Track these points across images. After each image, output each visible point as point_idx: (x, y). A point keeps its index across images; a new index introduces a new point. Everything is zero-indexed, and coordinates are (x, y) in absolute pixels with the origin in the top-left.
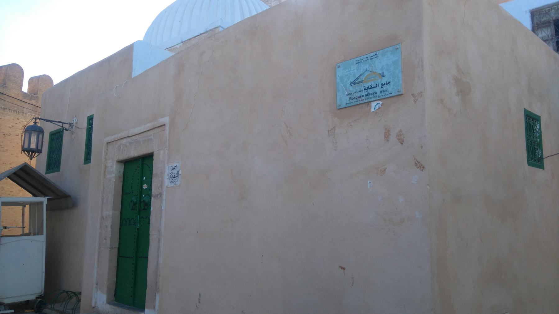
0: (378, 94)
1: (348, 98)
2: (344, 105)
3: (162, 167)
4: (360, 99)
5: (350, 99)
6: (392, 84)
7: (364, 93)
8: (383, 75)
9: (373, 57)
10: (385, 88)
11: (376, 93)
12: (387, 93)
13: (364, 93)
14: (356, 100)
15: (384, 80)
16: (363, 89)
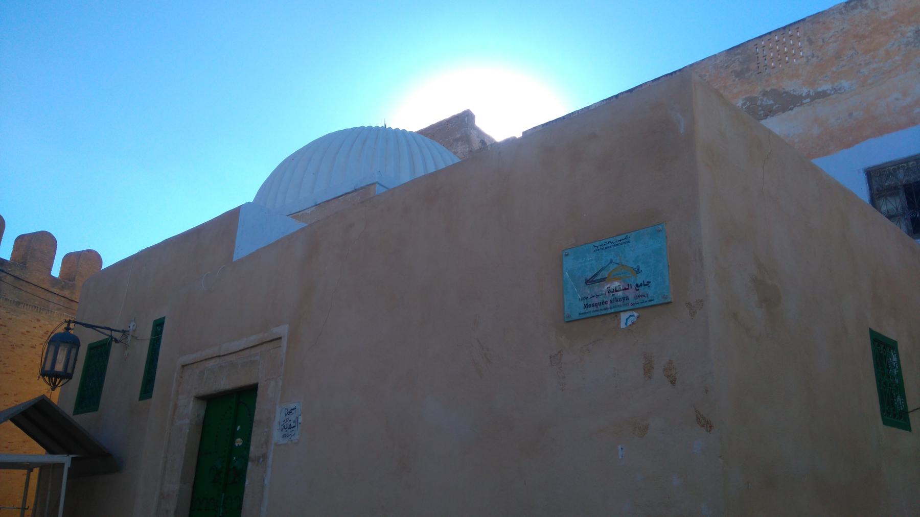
1: (582, 304)
2: (575, 316)
3: (271, 410)
4: (602, 307)
5: (586, 306)
6: (653, 284)
8: (638, 271)
10: (642, 290)
11: (628, 298)
12: (645, 299)
14: (595, 308)
15: (640, 279)
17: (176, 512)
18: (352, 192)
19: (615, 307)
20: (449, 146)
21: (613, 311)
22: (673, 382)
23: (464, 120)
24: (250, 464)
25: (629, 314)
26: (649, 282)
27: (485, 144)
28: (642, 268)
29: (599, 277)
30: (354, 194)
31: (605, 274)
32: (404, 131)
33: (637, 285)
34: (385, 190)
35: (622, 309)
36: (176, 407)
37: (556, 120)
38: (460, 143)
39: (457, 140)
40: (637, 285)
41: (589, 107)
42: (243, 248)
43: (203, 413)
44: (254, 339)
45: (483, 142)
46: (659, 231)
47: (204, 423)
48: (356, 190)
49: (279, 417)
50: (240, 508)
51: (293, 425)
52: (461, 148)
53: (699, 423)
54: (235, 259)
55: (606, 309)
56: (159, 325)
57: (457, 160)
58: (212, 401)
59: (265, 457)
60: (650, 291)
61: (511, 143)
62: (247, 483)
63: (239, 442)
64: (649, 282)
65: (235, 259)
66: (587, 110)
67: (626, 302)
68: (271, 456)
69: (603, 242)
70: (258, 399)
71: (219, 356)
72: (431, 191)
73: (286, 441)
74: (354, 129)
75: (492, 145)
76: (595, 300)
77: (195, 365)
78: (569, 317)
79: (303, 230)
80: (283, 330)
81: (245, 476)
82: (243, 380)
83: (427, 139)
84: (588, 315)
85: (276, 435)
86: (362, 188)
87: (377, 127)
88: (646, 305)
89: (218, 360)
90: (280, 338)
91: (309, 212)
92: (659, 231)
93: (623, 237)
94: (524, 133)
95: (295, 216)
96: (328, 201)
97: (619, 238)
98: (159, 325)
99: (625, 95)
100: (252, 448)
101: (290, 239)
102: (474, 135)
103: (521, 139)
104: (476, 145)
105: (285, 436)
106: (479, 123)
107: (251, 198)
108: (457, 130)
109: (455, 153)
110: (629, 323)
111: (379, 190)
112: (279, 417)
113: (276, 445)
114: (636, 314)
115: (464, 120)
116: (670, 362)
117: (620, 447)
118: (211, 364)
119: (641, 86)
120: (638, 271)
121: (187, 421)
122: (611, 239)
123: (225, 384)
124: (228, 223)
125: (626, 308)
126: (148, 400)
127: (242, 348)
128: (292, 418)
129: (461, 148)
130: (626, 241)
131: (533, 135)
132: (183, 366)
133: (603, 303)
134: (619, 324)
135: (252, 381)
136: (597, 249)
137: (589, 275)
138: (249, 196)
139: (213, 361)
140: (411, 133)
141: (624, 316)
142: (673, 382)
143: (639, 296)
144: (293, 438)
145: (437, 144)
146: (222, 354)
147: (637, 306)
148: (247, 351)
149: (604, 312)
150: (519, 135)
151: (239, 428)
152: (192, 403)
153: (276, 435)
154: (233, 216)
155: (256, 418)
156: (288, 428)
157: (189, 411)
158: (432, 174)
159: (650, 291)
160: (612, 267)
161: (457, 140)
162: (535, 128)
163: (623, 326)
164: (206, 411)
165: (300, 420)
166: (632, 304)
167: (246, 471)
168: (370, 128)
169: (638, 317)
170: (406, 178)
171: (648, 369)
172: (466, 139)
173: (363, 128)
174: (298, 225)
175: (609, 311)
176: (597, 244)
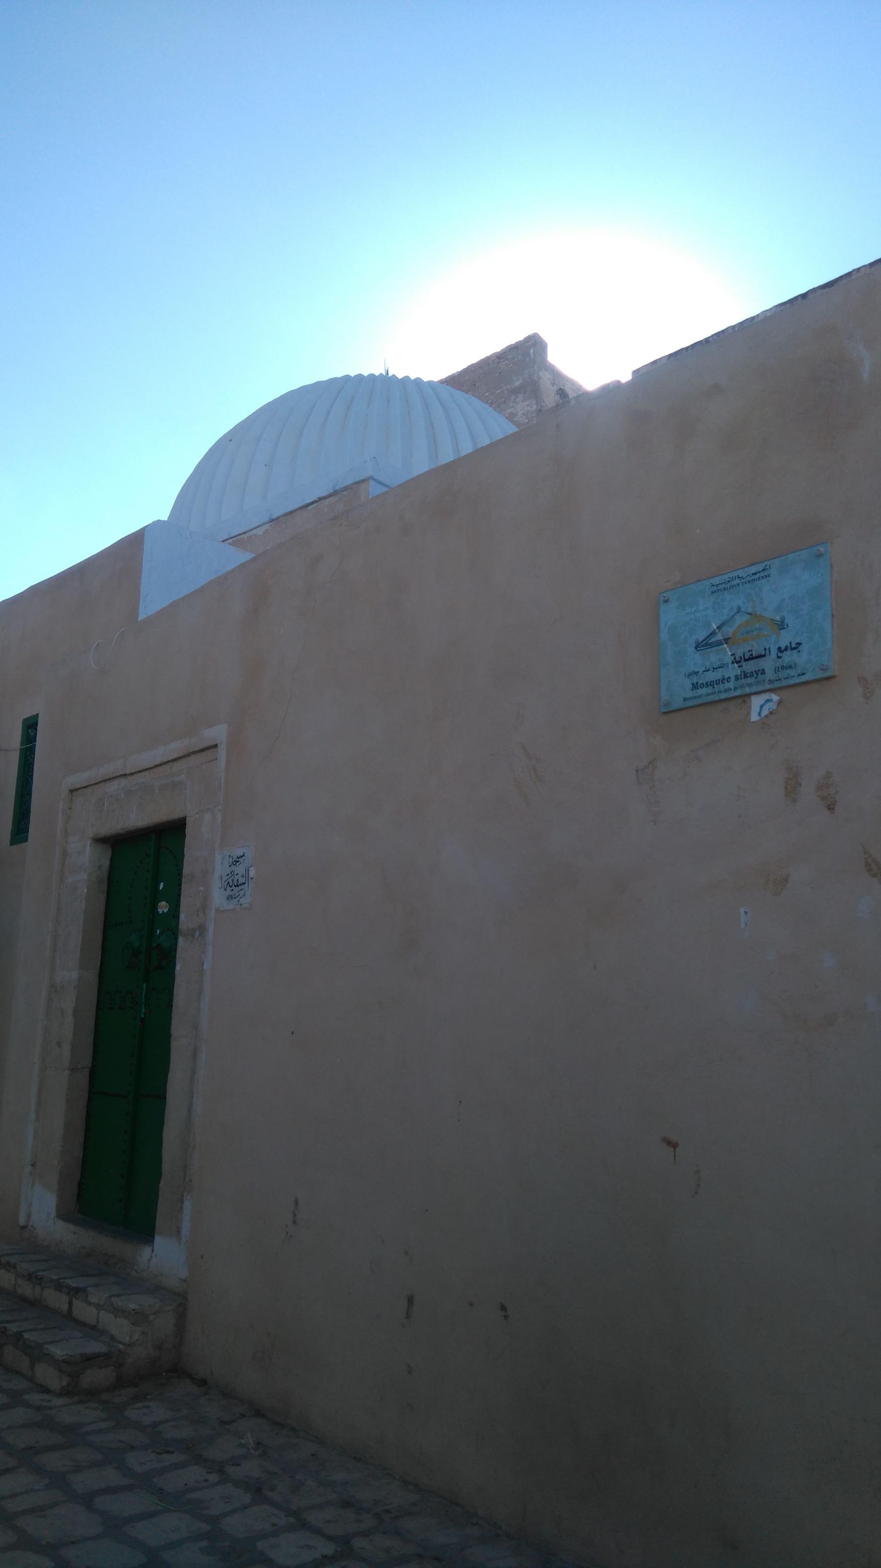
0: (770, 674)
1: (688, 684)
2: (678, 703)
3: (207, 857)
4: (722, 687)
5: (695, 686)
6: (805, 648)
7: (733, 671)
8: (782, 625)
9: (755, 578)
10: (787, 657)
11: (763, 672)
12: (791, 672)
13: (733, 671)
14: (709, 690)
15: (786, 638)
16: (729, 659)
17: (75, 1012)
18: (330, 496)
19: (742, 686)
20: (497, 403)
21: (738, 693)
22: (831, 808)
23: (527, 354)
24: (181, 940)
25: (765, 696)
26: (799, 644)
27: (565, 393)
28: (790, 620)
29: (719, 637)
30: (333, 500)
31: (729, 631)
32: (418, 382)
33: (779, 649)
34: (382, 490)
35: (754, 689)
36: (65, 854)
37: (693, 346)
38: (521, 396)
39: (516, 391)
40: (779, 649)
41: (753, 318)
42: (153, 599)
43: (106, 863)
44: (176, 747)
45: (562, 393)
46: (820, 555)
47: (109, 878)
48: (335, 493)
49: (220, 869)
50: (170, 1005)
51: (241, 880)
52: (523, 407)
53: (869, 870)
54: (142, 616)
55: (727, 690)
56: (31, 726)
57: (511, 429)
58: (119, 844)
59: (202, 929)
60: (801, 659)
61: (612, 391)
62: (178, 967)
63: (163, 907)
64: (799, 644)
65: (142, 616)
66: (750, 322)
67: (760, 677)
68: (211, 928)
69: (726, 577)
70: (188, 840)
71: (125, 775)
72: (451, 496)
73: (232, 905)
74: (332, 381)
75: (577, 398)
76: (712, 676)
77: (89, 790)
78: (667, 704)
79: (242, 566)
80: (219, 733)
81: (174, 957)
82: (157, 813)
83: (460, 396)
84: (700, 701)
85: (218, 897)
86: (346, 488)
87: (372, 376)
88: (792, 682)
89: (124, 782)
90: (216, 746)
91: (259, 532)
92: (820, 555)
93: (760, 567)
94: (635, 373)
95: (237, 540)
96: (291, 513)
97: (754, 569)
98: (31, 726)
99: (783, 307)
100: (182, 917)
101: (222, 583)
102: (545, 378)
103: (629, 384)
104: (550, 399)
105: (230, 898)
106: (555, 357)
107: (163, 513)
108: (515, 372)
109: (511, 418)
110: (765, 712)
111: (374, 490)
112: (220, 869)
113: (218, 910)
114: (775, 698)
115: (527, 354)
116: (829, 775)
117: (742, 910)
118: (113, 788)
119: (849, 274)
120: (782, 625)
121: (84, 876)
122: (740, 573)
123: (137, 817)
124: (125, 558)
125: (760, 688)
126: (24, 844)
127: (158, 762)
128: (240, 869)
129: (523, 407)
130: (764, 574)
131: (658, 377)
132: (71, 791)
133: (723, 680)
134: (748, 714)
135: (176, 815)
136: (717, 590)
137: (701, 635)
138: (160, 509)
139: (116, 782)
140: (430, 383)
141: (756, 702)
142: (831, 808)
143: (783, 668)
144: (242, 901)
145: (476, 402)
146: (128, 772)
147: (778, 684)
148: (167, 767)
149: (723, 696)
150: (625, 377)
151: (161, 886)
152: (88, 849)
153: (218, 897)
154: (131, 548)
155: (187, 870)
156: (234, 885)
157: (85, 863)
158: (447, 467)
159: (801, 659)
160: (740, 620)
161: (516, 391)
162: (654, 363)
163: (754, 717)
164: (112, 860)
165: (252, 873)
166: (771, 682)
167: (175, 950)
168: (360, 377)
169: (780, 703)
170: (421, 465)
171: (792, 788)
172: (532, 389)
173: (347, 378)
174: (238, 557)
175: (733, 694)
176: (716, 581)
